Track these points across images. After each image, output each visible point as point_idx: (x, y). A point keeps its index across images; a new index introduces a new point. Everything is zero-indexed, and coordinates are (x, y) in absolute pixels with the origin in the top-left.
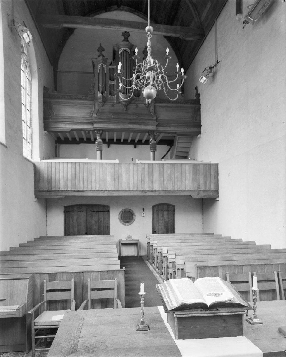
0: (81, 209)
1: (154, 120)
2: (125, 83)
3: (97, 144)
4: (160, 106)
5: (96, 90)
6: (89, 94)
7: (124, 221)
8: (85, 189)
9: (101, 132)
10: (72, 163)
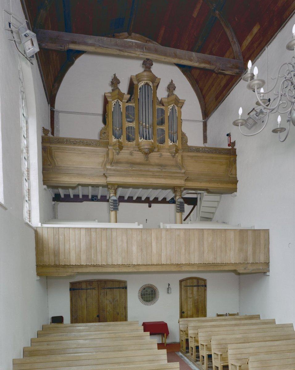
0: (91, 285)
2: (147, 125)
7: (144, 300)
8: (104, 263)
10: (86, 228)
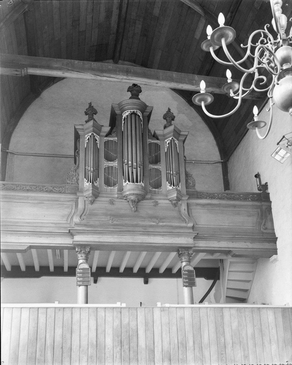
1: (189, 228)
3: (80, 273)
4: (198, 204)
5: (82, 175)
6: (67, 183)
9: (88, 249)
